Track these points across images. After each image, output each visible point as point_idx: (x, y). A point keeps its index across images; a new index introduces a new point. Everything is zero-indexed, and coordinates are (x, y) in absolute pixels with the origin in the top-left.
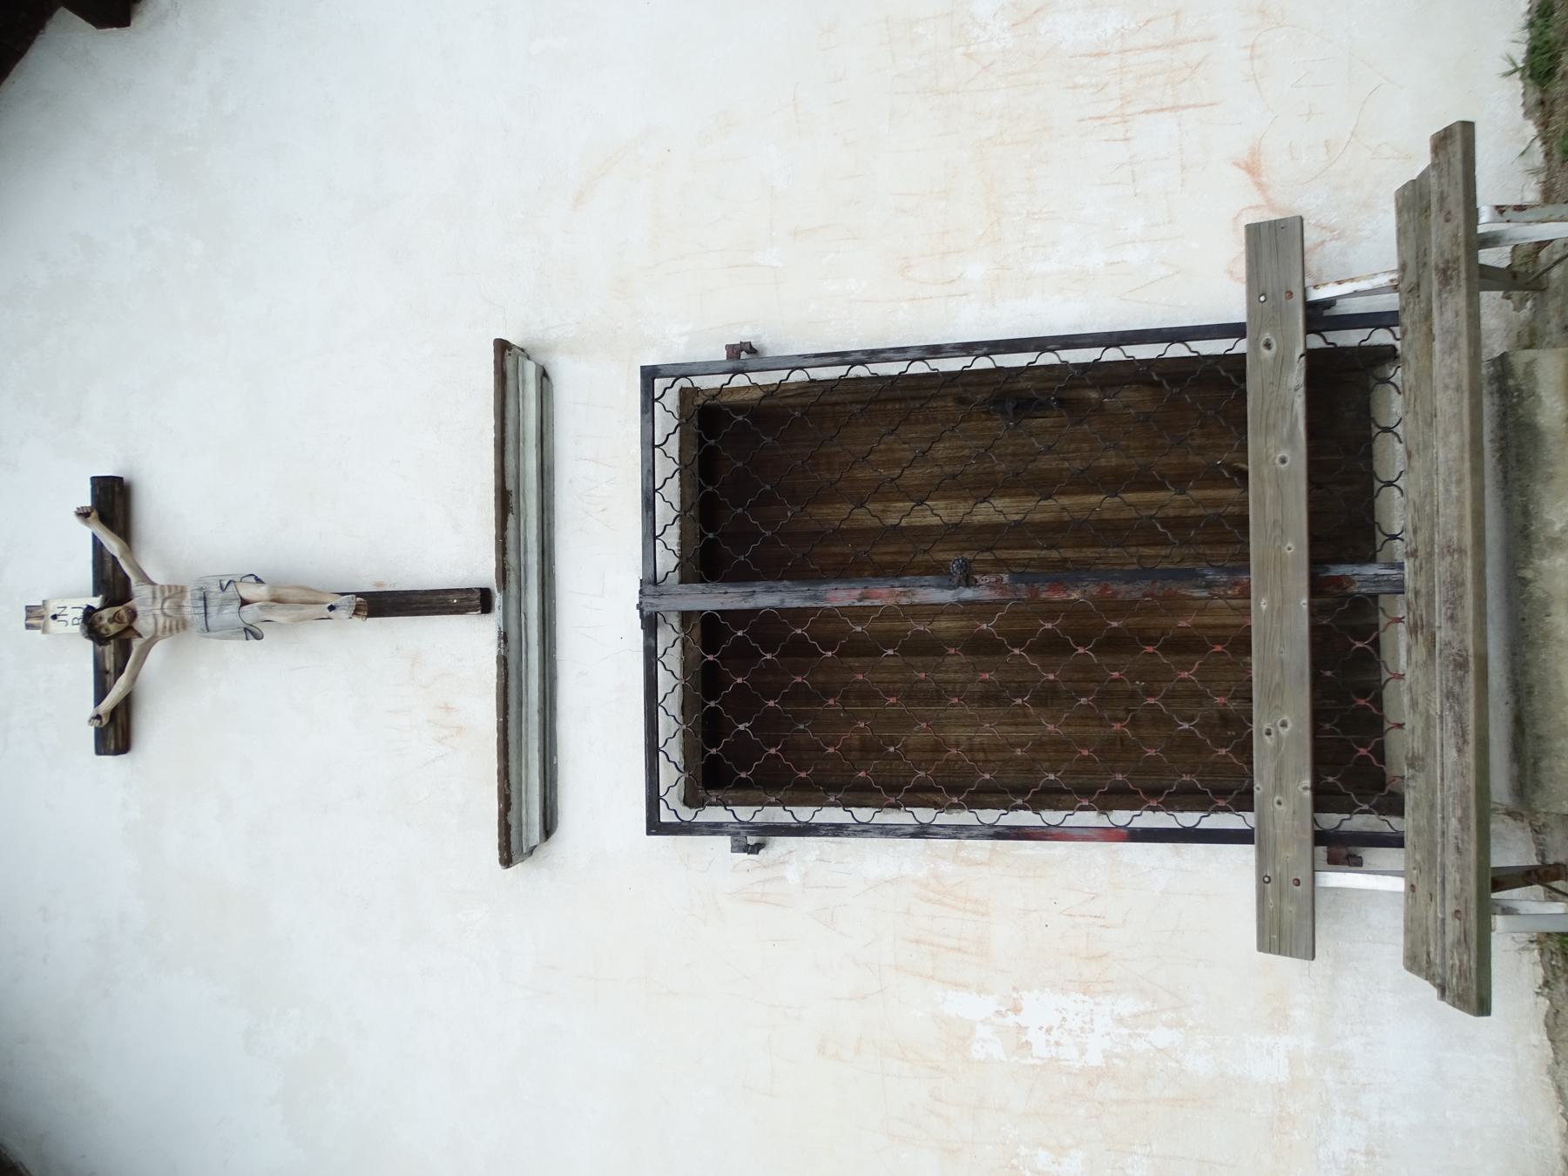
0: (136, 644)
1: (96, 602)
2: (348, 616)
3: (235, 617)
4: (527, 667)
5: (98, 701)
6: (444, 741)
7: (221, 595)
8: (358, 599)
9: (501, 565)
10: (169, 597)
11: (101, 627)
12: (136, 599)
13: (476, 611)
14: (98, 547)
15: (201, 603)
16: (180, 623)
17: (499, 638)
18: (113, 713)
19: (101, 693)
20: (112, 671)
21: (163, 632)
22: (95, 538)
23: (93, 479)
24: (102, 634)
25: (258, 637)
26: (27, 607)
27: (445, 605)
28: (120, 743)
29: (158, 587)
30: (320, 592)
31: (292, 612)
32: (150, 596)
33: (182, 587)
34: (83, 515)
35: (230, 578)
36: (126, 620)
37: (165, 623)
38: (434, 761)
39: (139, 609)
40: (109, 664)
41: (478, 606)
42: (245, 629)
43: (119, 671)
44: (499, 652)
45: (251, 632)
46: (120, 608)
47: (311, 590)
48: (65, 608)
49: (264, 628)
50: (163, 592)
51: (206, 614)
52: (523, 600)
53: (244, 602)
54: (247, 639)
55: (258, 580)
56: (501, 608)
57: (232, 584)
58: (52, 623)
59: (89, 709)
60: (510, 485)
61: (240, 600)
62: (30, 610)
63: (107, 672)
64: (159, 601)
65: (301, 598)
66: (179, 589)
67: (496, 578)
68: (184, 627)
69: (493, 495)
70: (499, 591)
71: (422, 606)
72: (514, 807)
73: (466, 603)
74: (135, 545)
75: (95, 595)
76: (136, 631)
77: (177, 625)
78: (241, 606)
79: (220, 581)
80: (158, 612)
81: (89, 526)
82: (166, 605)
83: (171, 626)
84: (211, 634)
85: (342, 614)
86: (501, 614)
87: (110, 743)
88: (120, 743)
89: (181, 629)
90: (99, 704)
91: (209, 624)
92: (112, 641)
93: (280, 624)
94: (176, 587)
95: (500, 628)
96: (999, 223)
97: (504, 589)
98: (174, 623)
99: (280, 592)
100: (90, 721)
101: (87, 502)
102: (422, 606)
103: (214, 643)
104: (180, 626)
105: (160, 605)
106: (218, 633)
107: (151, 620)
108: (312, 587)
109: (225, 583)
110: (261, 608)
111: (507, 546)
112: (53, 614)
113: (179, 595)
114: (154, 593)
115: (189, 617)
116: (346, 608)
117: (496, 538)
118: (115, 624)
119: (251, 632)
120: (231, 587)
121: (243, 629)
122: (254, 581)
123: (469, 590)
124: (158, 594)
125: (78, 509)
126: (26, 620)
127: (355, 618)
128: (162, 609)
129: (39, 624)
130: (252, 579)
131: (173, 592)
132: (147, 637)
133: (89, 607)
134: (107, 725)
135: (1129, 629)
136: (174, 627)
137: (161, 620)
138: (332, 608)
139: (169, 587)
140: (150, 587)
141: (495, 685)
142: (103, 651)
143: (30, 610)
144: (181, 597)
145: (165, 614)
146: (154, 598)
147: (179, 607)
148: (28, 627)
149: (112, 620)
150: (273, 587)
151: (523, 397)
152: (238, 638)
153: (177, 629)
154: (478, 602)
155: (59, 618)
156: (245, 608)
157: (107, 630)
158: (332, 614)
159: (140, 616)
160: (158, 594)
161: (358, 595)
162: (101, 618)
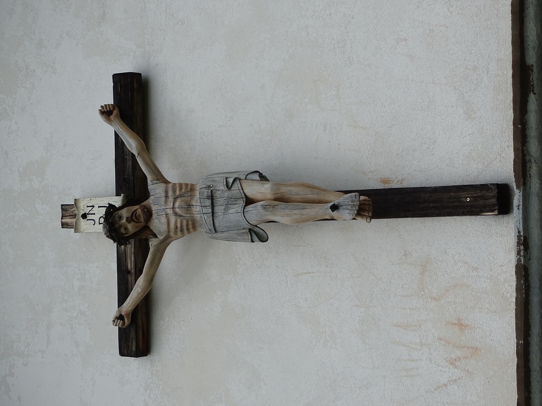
0: (153, 243)
1: (117, 201)
2: (352, 217)
3: (240, 217)
5: (121, 301)
6: (457, 364)
7: (227, 194)
8: (362, 198)
9: (520, 155)
10: (180, 196)
11: (120, 226)
12: (152, 198)
13: (493, 211)
14: (119, 145)
15: (208, 202)
16: (190, 223)
17: (519, 244)
18: (134, 313)
19: (122, 297)
20: (133, 271)
21: (176, 233)
22: (117, 136)
23: (115, 76)
24: (122, 234)
25: (263, 239)
26: (62, 205)
27: (456, 204)
28: (141, 344)
29: (170, 185)
30: (324, 190)
31: (294, 212)
32: (163, 195)
33: (192, 185)
34: (106, 112)
35: (236, 176)
36: (142, 220)
37: (176, 221)
38: (445, 385)
39: (154, 208)
40: (130, 265)
41: (494, 205)
42: (250, 230)
43: (139, 272)
44: (519, 260)
45: (257, 234)
46: (137, 207)
47: (314, 187)
48: (93, 206)
49: (269, 229)
50: (174, 191)
51: (213, 213)
53: (249, 201)
54: (252, 241)
55: (263, 178)
56: (521, 207)
57: (238, 182)
58: (83, 222)
59: (113, 309)
61: (244, 199)
62: (64, 208)
63: (129, 272)
64: (171, 200)
65: (305, 196)
66: (189, 187)
67: (514, 171)
68: (194, 228)
69: (510, 72)
70: (518, 187)
71: (431, 205)
73: (481, 202)
74: (153, 143)
75: (118, 194)
76: (151, 231)
77: (187, 225)
78: (246, 206)
79: (226, 178)
80: (170, 211)
81: (111, 125)
82: (177, 204)
83: (182, 226)
84: (219, 235)
85: (346, 214)
86: (521, 215)
87: (132, 344)
88: (141, 344)
89: (191, 230)
90: (122, 304)
91: (217, 225)
92: (132, 241)
93: (285, 226)
94: (187, 185)
95: (519, 232)
96: (420, 326)
97: (525, 184)
98: (185, 223)
99: (285, 190)
100: (114, 321)
101: (109, 100)
102: (431, 205)
103: (223, 244)
104: (190, 226)
105: (172, 204)
106: (225, 234)
107: (164, 220)
108: (317, 185)
109: (231, 180)
110: (265, 207)
111: (528, 132)
112: (83, 213)
113: (189, 194)
114: (166, 192)
115: (198, 217)
116: (349, 207)
117: (514, 124)
118: (132, 223)
119: (257, 234)
120: (237, 185)
121: (247, 231)
122: (259, 179)
123: (484, 187)
124: (170, 193)
125: (102, 106)
126: (62, 219)
127: (359, 219)
128: (173, 208)
129: (72, 223)
130: (256, 177)
131: (183, 190)
132: (161, 238)
133: (111, 206)
134: (129, 326)
135: (127, 198)
136: (185, 227)
137: (173, 219)
138: (334, 208)
139: (181, 185)
140: (163, 185)
141: (514, 300)
142: (125, 251)
143: (64, 208)
144: (191, 196)
145: (176, 214)
146: (167, 197)
147: (189, 206)
148: (64, 225)
149: (129, 220)
150: (278, 185)
152: (244, 240)
153: (188, 229)
154: (494, 201)
155: (89, 217)
156: (250, 208)
157: (126, 229)
158: (335, 214)
159: (154, 216)
160: (170, 193)
161: (362, 192)
162: (121, 218)
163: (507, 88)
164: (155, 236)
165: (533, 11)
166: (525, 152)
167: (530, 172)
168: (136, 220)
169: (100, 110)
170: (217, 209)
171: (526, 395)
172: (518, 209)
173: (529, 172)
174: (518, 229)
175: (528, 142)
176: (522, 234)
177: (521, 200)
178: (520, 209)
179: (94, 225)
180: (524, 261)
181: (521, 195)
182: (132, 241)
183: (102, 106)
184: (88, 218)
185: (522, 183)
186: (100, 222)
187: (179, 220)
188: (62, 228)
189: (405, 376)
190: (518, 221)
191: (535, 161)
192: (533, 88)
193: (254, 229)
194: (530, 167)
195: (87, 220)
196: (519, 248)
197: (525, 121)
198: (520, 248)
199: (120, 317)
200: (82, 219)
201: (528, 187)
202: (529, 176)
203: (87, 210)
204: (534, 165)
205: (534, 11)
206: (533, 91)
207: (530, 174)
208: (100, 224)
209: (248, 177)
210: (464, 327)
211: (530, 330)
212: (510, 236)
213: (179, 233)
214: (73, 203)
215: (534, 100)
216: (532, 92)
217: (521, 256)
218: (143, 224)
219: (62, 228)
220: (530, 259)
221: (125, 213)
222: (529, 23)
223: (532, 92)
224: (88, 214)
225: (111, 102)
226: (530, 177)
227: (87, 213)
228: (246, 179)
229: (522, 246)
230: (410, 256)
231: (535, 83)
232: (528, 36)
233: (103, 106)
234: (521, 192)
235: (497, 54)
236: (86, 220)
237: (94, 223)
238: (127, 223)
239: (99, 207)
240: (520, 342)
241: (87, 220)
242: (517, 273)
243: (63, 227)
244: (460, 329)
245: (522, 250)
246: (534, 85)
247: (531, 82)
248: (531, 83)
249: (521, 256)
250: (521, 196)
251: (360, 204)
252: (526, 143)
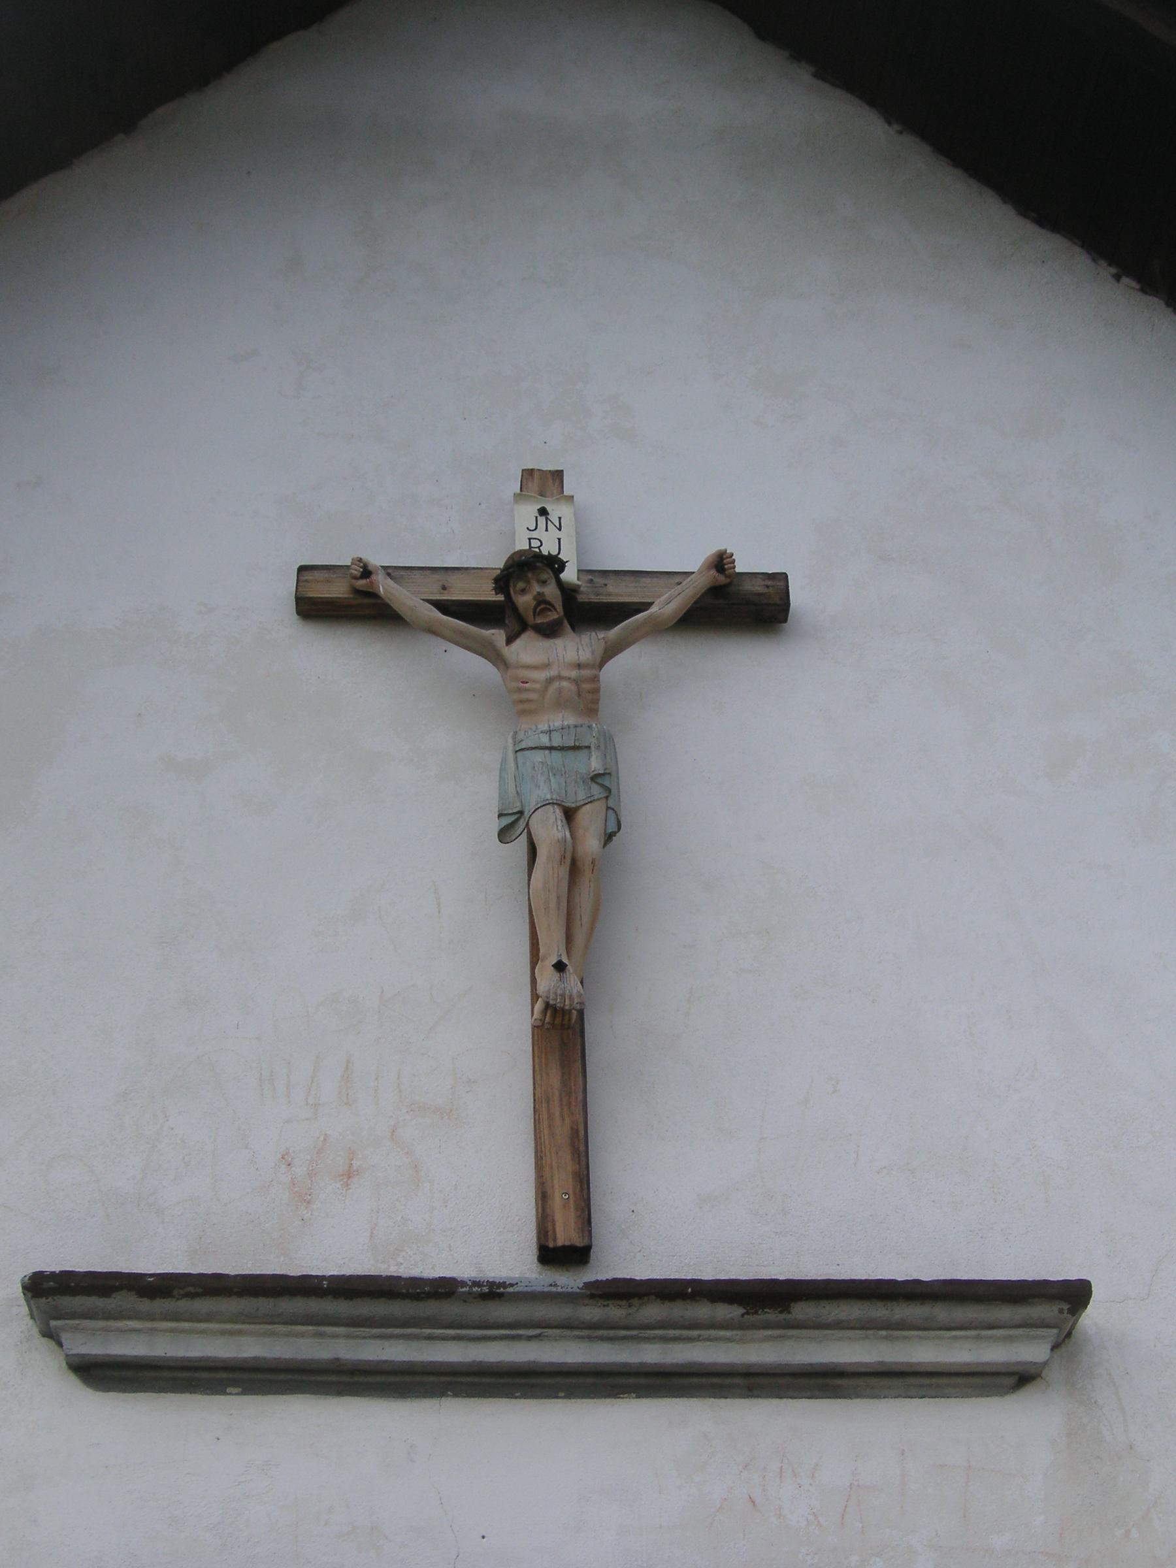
0: (497, 636)
4: (430, 1338)
11: (528, 582)
17: (491, 1284)
23: (784, 577)
24: (515, 586)
25: (504, 834)
34: (721, 562)
36: (539, 621)
44: (463, 1283)
52: (568, 1332)
54: (500, 815)
55: (609, 837)
56: (553, 1289)
58: (531, 509)
60: (802, 1310)
68: (523, 713)
72: (145, 1305)
77: (529, 701)
80: (553, 672)
83: (526, 690)
85: (547, 980)
89: (516, 696)
95: (511, 1285)
97: (592, 1296)
100: (360, 560)
118: (534, 603)
130: (612, 827)
133: (562, 565)
137: (541, 676)
145: (550, 681)
151: (978, 1337)
152: (502, 796)
155: (542, 520)
156: (559, 812)
157: (523, 591)
163: (750, 1266)
164: (510, 640)
165: (878, 1315)
166: (646, 1298)
167: (611, 1306)
168: (540, 610)
169: (726, 550)
170: (557, 755)
171: (235, 1290)
172: (551, 1285)
173: (613, 1304)
174: (517, 1284)
175: (663, 1303)
176: (510, 1290)
177: (564, 1290)
178: (550, 1287)
179: (528, 528)
180: (464, 1293)
181: (574, 1290)
182: (501, 598)
183: (733, 555)
184: (539, 518)
185: (593, 1292)
186: (532, 540)
187: (537, 686)
188: (523, 470)
189: (261, 1074)
190: (530, 1284)
191: (630, 1314)
192: (753, 1314)
193: (522, 820)
194: (620, 1306)
195: (536, 517)
196: (485, 1284)
197: (698, 1298)
198: (485, 1286)
199: (367, 573)
200: (539, 507)
201: (586, 1302)
202: (605, 1303)
203: (554, 517)
204: (623, 1313)
205: (880, 1317)
206: (747, 1313)
207: (608, 1305)
208: (530, 539)
209: (610, 812)
210: (345, 1180)
211: (345, 1299)
212: (501, 1265)
213: (514, 685)
214: (566, 493)
215: (731, 1315)
216: (745, 1311)
217: (470, 1287)
218: (531, 620)
219: (523, 470)
220: (465, 1301)
221: (551, 591)
222: (249, 173)
223: (745, 1311)
224: (547, 519)
225: (738, 570)
226: (604, 1306)
227: (549, 517)
228: (608, 808)
229: (487, 1290)
230: (468, 1090)
231: (760, 1317)
232: (838, 1307)
233: (733, 557)
234: (578, 1290)
235: (808, 1250)
236: (538, 515)
237: (530, 528)
238: (535, 593)
239: (559, 539)
240: (324, 1282)
241: (536, 517)
242: (442, 1280)
243: (524, 472)
244: (343, 1175)
245: (481, 1290)
246: (758, 1314)
247: (763, 1310)
248: (761, 1310)
249: (470, 1287)
250: (571, 1290)
251: (563, 1010)
252: (661, 1300)
